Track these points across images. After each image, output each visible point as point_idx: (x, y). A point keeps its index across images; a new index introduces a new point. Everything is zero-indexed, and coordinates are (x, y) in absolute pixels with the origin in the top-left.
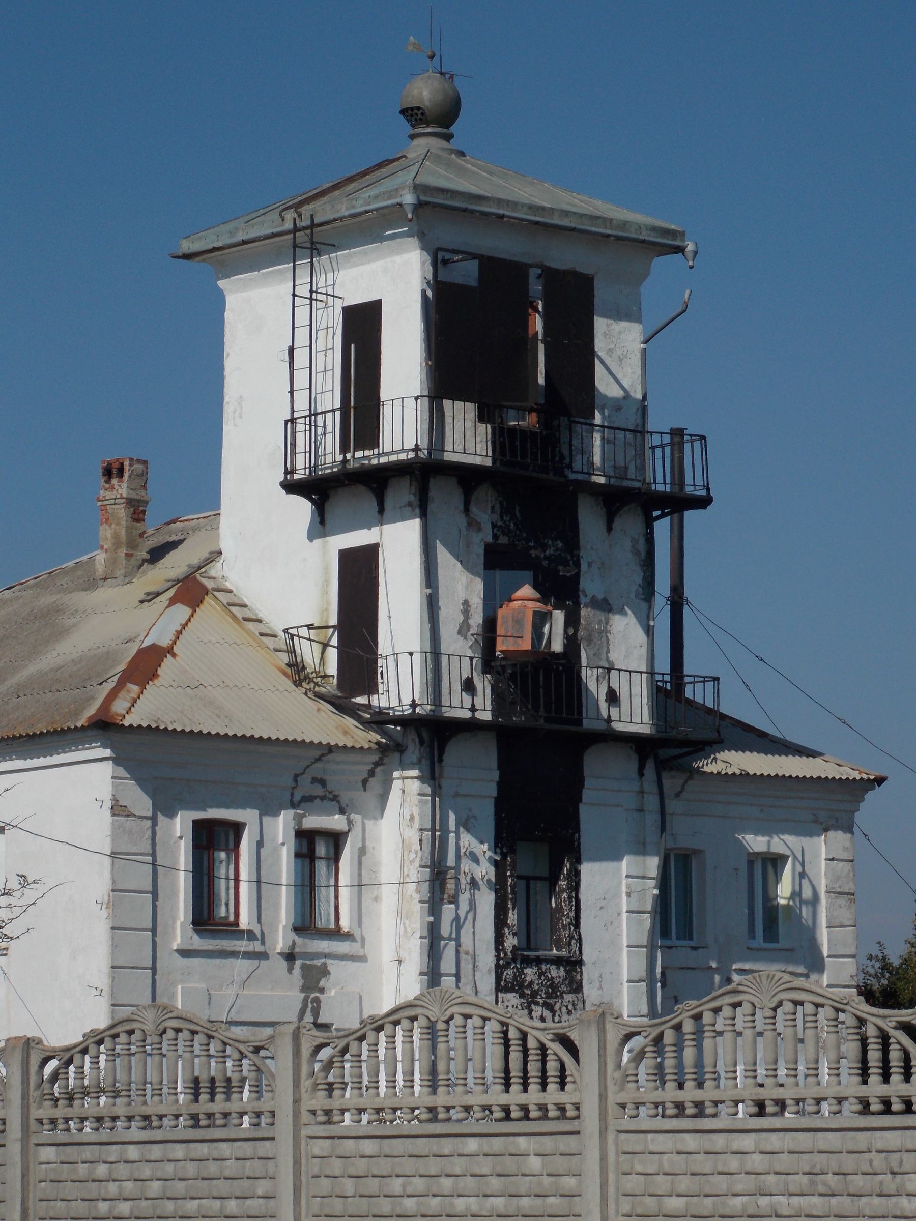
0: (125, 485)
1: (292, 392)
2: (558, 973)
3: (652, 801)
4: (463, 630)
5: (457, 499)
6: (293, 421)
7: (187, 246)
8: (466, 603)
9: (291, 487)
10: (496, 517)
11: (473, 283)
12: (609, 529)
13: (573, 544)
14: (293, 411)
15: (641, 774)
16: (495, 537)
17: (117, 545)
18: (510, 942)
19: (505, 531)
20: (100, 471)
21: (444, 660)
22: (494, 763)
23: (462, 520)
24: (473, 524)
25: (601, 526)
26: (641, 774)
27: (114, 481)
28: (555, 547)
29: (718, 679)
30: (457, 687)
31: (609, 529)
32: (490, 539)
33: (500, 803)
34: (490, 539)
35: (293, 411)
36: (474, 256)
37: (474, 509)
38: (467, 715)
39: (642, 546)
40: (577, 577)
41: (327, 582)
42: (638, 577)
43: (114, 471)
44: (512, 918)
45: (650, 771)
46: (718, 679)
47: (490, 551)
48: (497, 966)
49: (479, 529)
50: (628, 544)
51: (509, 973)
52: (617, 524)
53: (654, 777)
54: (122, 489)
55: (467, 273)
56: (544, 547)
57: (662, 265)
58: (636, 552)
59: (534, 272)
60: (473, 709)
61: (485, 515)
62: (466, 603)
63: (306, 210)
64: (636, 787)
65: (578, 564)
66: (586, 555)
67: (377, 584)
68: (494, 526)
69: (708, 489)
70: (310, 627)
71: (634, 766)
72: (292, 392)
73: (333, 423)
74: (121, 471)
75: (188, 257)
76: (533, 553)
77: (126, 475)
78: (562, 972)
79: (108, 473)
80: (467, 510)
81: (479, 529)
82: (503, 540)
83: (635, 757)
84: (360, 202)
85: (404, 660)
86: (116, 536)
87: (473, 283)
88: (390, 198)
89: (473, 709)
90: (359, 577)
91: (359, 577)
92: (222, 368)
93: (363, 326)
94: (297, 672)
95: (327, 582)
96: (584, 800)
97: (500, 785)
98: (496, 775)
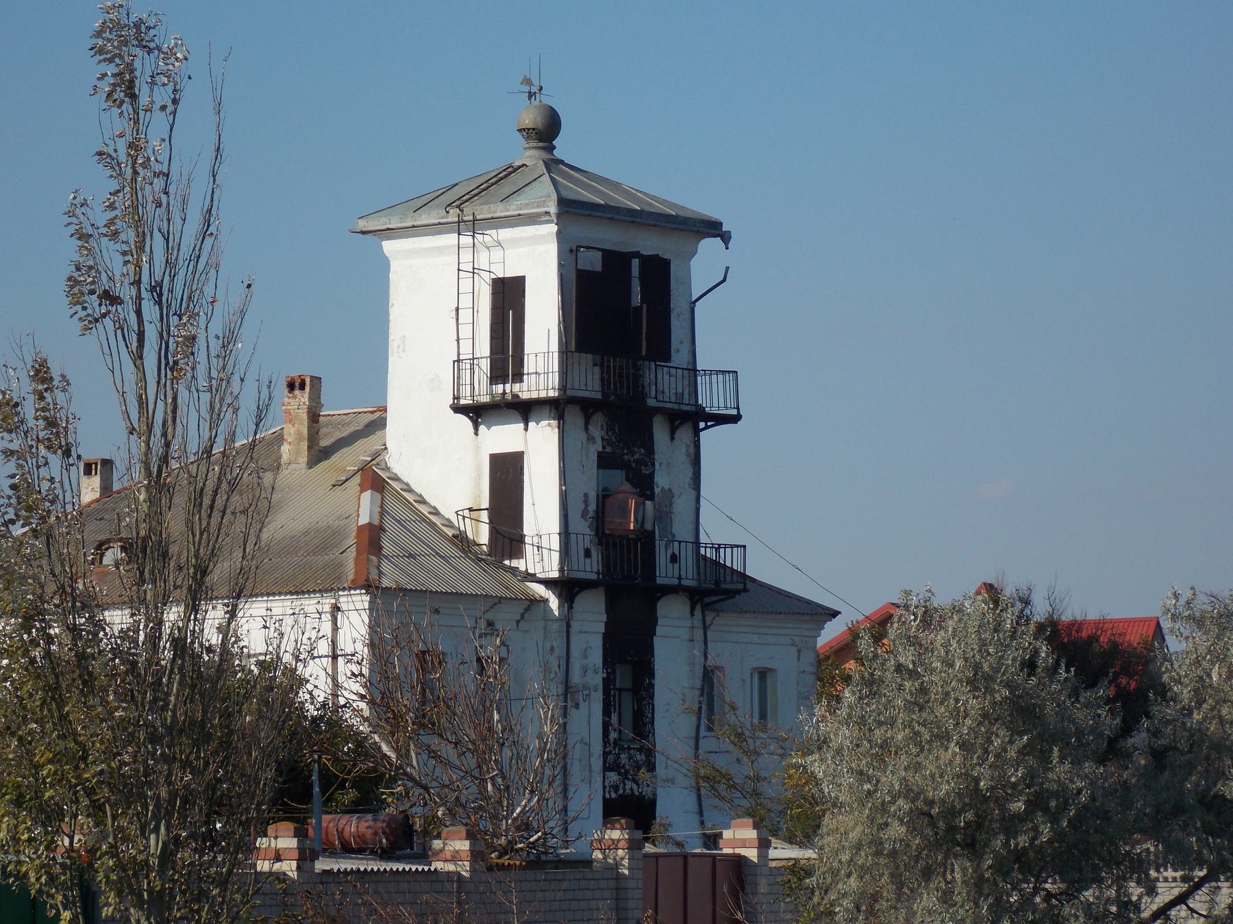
0: (306, 395)
1: (458, 340)
2: (640, 757)
3: (699, 634)
4: (584, 514)
5: (580, 422)
6: (458, 361)
7: (362, 225)
8: (586, 495)
9: (458, 409)
10: (603, 433)
11: (599, 268)
12: (672, 438)
13: (650, 452)
14: (459, 354)
15: (692, 614)
16: (604, 447)
17: (300, 439)
18: (613, 735)
19: (610, 443)
20: (285, 384)
21: (573, 537)
22: (603, 609)
23: (583, 436)
24: (591, 439)
25: (667, 436)
26: (692, 614)
27: (297, 392)
28: (640, 453)
29: (744, 547)
30: (582, 553)
31: (672, 438)
32: (600, 449)
33: (606, 636)
34: (600, 449)
35: (459, 354)
36: (599, 249)
37: (590, 427)
38: (676, 582)
39: (692, 450)
40: (653, 473)
41: (479, 476)
42: (689, 472)
43: (297, 384)
44: (614, 718)
45: (698, 612)
46: (744, 547)
47: (601, 456)
48: (604, 753)
49: (594, 442)
50: (684, 450)
51: (611, 758)
52: (678, 434)
53: (700, 617)
54: (303, 398)
55: (593, 261)
56: (633, 453)
57: (709, 245)
58: (688, 455)
59: (635, 262)
60: (680, 578)
61: (597, 432)
62: (586, 495)
63: (468, 208)
64: (688, 623)
65: (653, 465)
66: (658, 457)
67: (521, 481)
68: (603, 439)
69: (738, 409)
70: (470, 510)
71: (688, 608)
72: (458, 340)
73: (485, 365)
74: (302, 387)
75: (363, 233)
76: (626, 457)
77: (307, 388)
78: (643, 757)
79: (291, 386)
80: (586, 429)
81: (594, 442)
82: (609, 449)
83: (688, 602)
84: (513, 207)
85: (580, 537)
86: (299, 433)
87: (599, 268)
88: (538, 207)
89: (680, 578)
90: (507, 473)
91: (507, 473)
92: (387, 314)
93: (508, 296)
94: (461, 541)
95: (479, 476)
96: (600, 637)
97: (607, 624)
98: (604, 618)
